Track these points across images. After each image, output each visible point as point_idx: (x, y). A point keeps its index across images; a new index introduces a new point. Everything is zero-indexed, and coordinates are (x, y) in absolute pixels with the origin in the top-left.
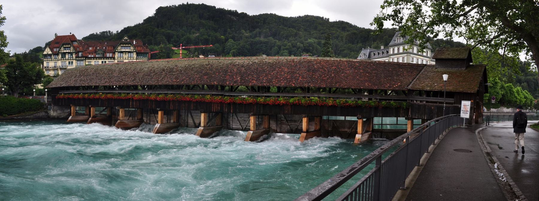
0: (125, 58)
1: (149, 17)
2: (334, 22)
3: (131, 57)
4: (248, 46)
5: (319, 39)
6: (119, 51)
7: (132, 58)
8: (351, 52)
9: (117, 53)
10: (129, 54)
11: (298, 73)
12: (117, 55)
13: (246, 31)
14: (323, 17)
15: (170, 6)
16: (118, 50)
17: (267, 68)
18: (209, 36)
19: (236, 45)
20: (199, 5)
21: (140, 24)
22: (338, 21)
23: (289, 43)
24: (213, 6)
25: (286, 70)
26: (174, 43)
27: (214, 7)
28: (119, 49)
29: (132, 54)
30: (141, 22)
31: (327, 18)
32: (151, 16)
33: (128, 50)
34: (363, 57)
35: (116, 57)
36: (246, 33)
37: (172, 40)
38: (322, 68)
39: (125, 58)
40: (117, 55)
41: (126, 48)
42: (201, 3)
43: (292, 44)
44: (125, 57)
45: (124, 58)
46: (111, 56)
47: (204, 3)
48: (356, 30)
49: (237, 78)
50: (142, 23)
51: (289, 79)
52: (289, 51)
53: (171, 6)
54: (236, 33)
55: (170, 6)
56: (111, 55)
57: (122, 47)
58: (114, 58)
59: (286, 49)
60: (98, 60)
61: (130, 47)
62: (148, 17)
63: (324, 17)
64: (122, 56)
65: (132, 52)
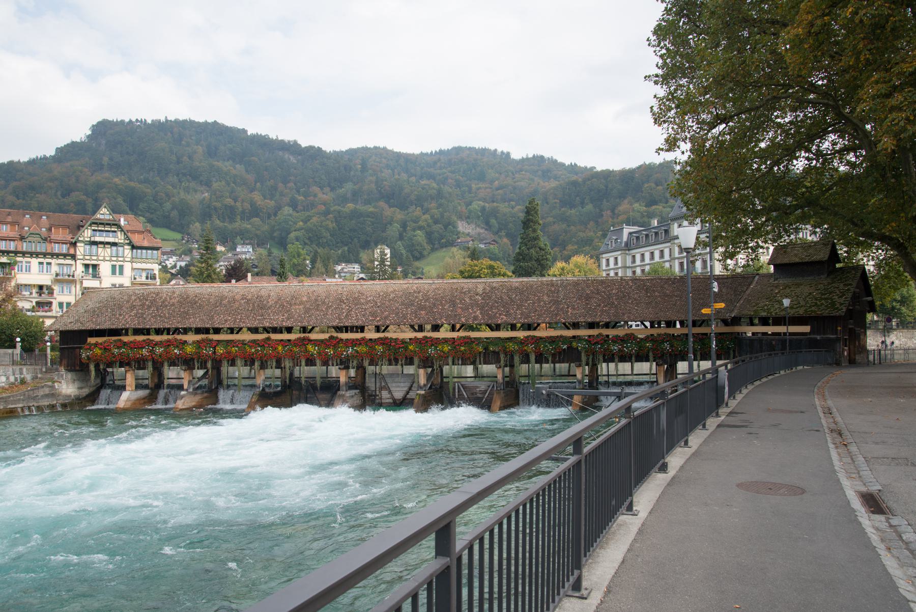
0: (104, 257)
1: (73, 142)
2: (523, 160)
3: (117, 257)
4: (331, 225)
5: (493, 202)
6: (87, 239)
7: (120, 259)
8: (569, 226)
9: (82, 245)
10: (114, 248)
11: (565, 302)
12: (82, 249)
13: (322, 189)
14: (496, 150)
15: (131, 121)
16: (83, 236)
17: (516, 295)
18: (235, 200)
19: (302, 221)
20: (206, 124)
21: (45, 158)
22: (530, 156)
23: (424, 214)
24: (240, 127)
25: (545, 298)
26: (148, 215)
27: (244, 131)
28: (87, 234)
29: (121, 249)
30: (51, 152)
31: (505, 151)
32: (78, 140)
33: (111, 240)
34: (614, 245)
35: (78, 253)
36: (324, 194)
37: (141, 206)
38: (598, 293)
39: (104, 257)
40: (81, 249)
41: (104, 234)
42: (210, 120)
43: (432, 217)
44: (102, 255)
45: (101, 258)
46: (64, 251)
47: (219, 121)
48: (577, 174)
49: (475, 312)
50: (53, 157)
51: (554, 311)
52: (426, 232)
53: (134, 120)
54: (298, 191)
55: (131, 121)
56: (64, 249)
57: (94, 230)
58: (74, 257)
59: (420, 228)
60: (29, 259)
61: (115, 232)
62: (69, 142)
63: (499, 150)
64: (120, 254)
65: (122, 245)
